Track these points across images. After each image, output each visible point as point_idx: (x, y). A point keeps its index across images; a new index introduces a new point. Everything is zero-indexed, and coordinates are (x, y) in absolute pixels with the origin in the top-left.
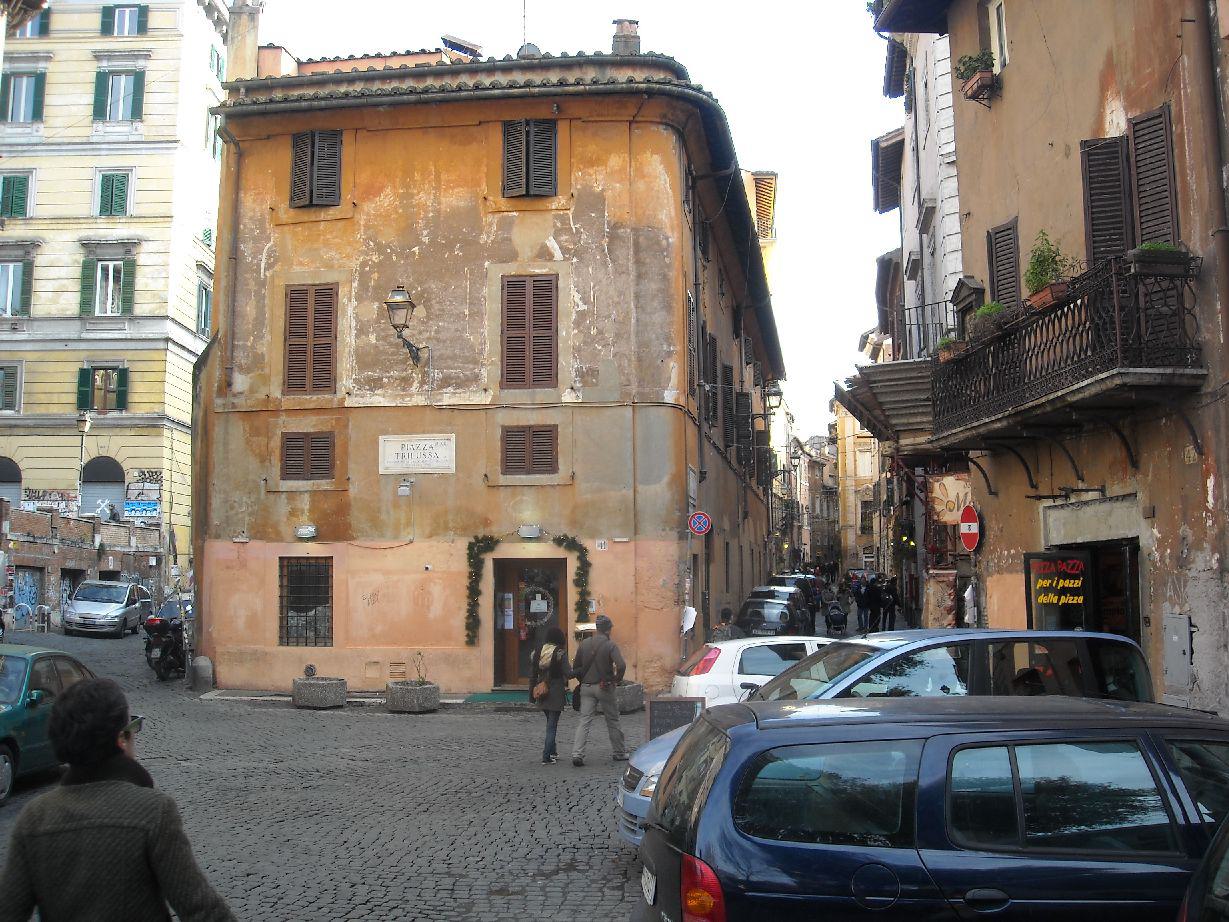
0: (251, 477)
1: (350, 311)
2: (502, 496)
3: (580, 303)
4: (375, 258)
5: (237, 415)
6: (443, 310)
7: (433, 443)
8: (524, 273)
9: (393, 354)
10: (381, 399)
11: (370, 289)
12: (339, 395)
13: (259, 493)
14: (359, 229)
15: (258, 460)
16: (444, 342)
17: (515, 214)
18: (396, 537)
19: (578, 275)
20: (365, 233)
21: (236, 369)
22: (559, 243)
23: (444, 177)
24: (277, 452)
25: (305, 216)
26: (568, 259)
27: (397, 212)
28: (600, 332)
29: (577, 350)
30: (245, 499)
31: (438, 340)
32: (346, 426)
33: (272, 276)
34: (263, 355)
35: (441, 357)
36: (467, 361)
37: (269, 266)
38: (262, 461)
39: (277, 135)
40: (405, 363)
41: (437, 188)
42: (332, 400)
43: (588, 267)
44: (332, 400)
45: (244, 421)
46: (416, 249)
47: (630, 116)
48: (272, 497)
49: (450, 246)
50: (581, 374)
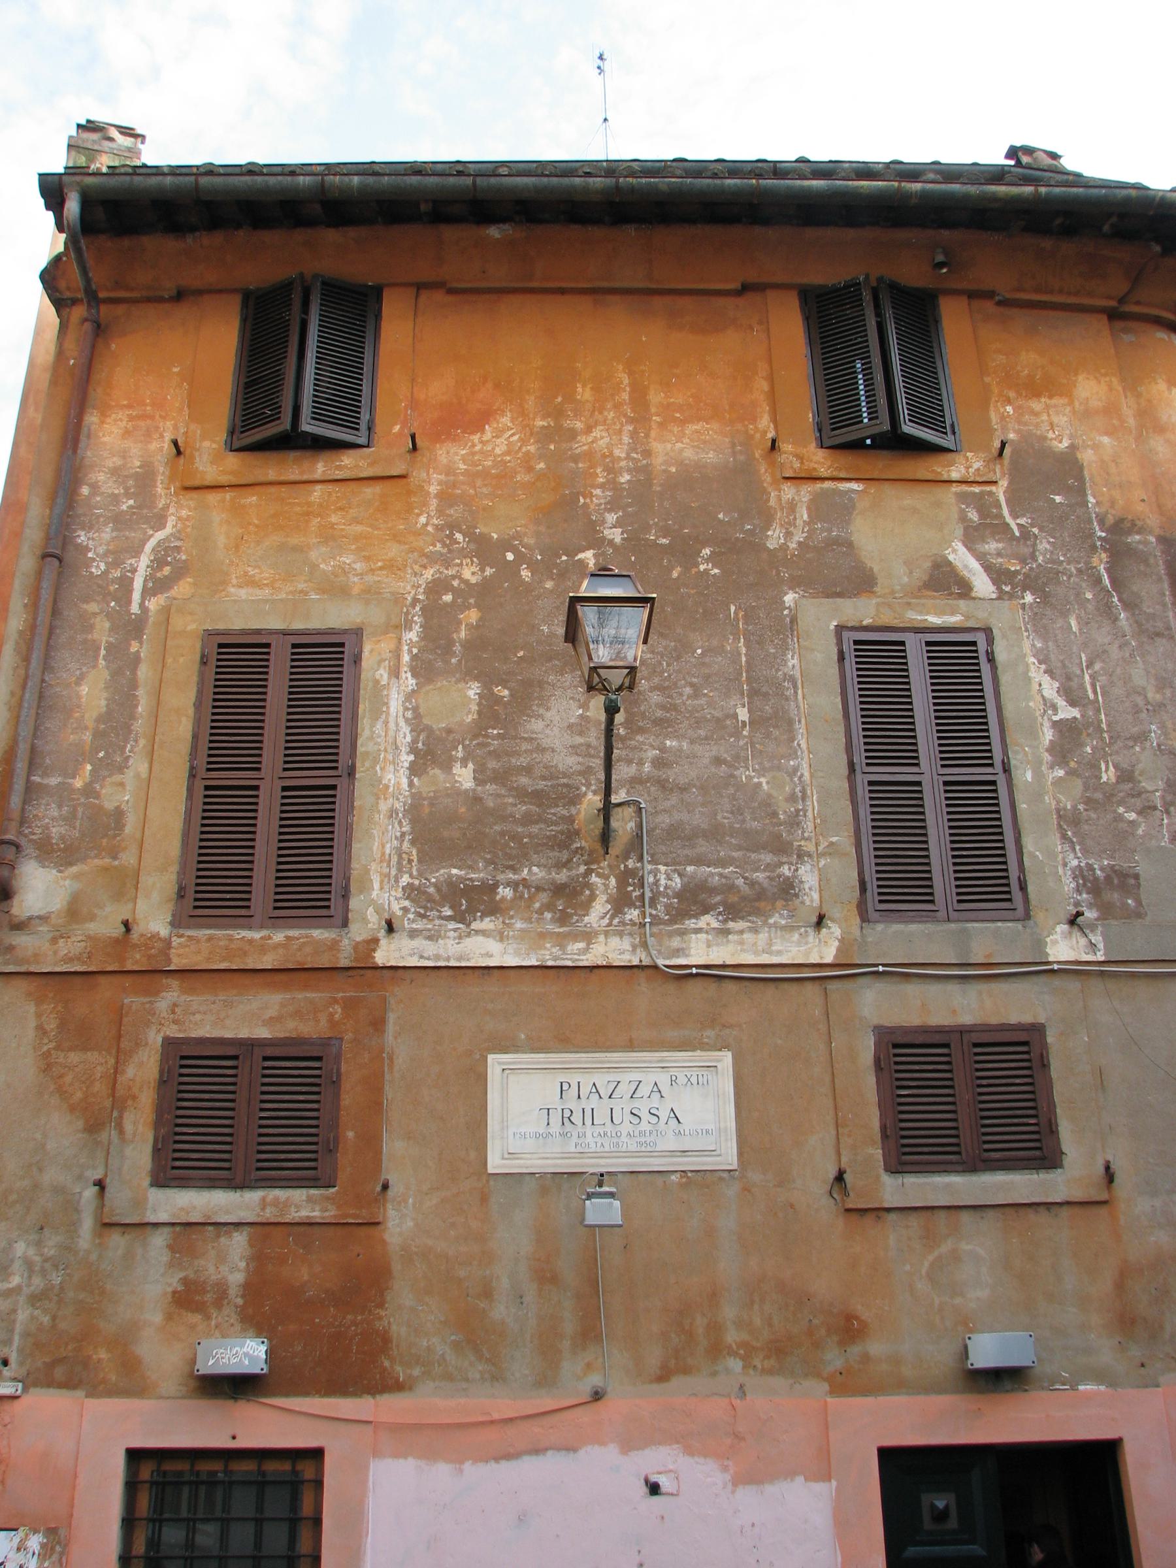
0: (52, 1175)
1: (395, 703)
2: (892, 1240)
3: (1061, 703)
4: (470, 573)
5: (22, 985)
6: (674, 708)
7: (663, 1079)
8: (896, 623)
9: (527, 820)
10: (493, 946)
11: (457, 648)
12: (358, 932)
13: (72, 1227)
14: (425, 504)
15: (80, 1124)
16: (683, 789)
17: (854, 486)
18: (546, 1380)
19: (1042, 631)
20: (440, 512)
21: (29, 850)
22: (981, 557)
23: (656, 397)
24: (147, 1099)
25: (271, 468)
26: (1011, 596)
27: (530, 469)
28: (1126, 775)
29: (1068, 821)
30: (20, 1248)
31: (662, 784)
32: (378, 1024)
33: (166, 611)
34: (119, 814)
35: (673, 832)
36: (753, 842)
37: (155, 586)
38: (93, 1127)
39: (200, 292)
40: (567, 847)
41: (640, 418)
42: (334, 946)
43: (1065, 614)
44: (334, 946)
45: (39, 1002)
46: (564, 558)
47: (1109, 297)
48: (117, 1241)
49: (686, 553)
50: (1086, 880)
